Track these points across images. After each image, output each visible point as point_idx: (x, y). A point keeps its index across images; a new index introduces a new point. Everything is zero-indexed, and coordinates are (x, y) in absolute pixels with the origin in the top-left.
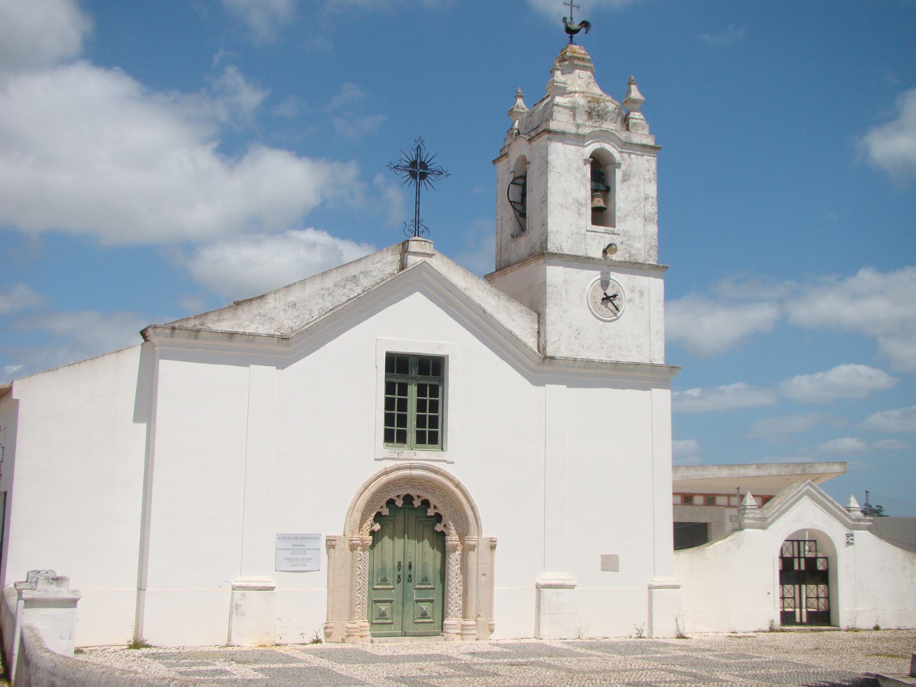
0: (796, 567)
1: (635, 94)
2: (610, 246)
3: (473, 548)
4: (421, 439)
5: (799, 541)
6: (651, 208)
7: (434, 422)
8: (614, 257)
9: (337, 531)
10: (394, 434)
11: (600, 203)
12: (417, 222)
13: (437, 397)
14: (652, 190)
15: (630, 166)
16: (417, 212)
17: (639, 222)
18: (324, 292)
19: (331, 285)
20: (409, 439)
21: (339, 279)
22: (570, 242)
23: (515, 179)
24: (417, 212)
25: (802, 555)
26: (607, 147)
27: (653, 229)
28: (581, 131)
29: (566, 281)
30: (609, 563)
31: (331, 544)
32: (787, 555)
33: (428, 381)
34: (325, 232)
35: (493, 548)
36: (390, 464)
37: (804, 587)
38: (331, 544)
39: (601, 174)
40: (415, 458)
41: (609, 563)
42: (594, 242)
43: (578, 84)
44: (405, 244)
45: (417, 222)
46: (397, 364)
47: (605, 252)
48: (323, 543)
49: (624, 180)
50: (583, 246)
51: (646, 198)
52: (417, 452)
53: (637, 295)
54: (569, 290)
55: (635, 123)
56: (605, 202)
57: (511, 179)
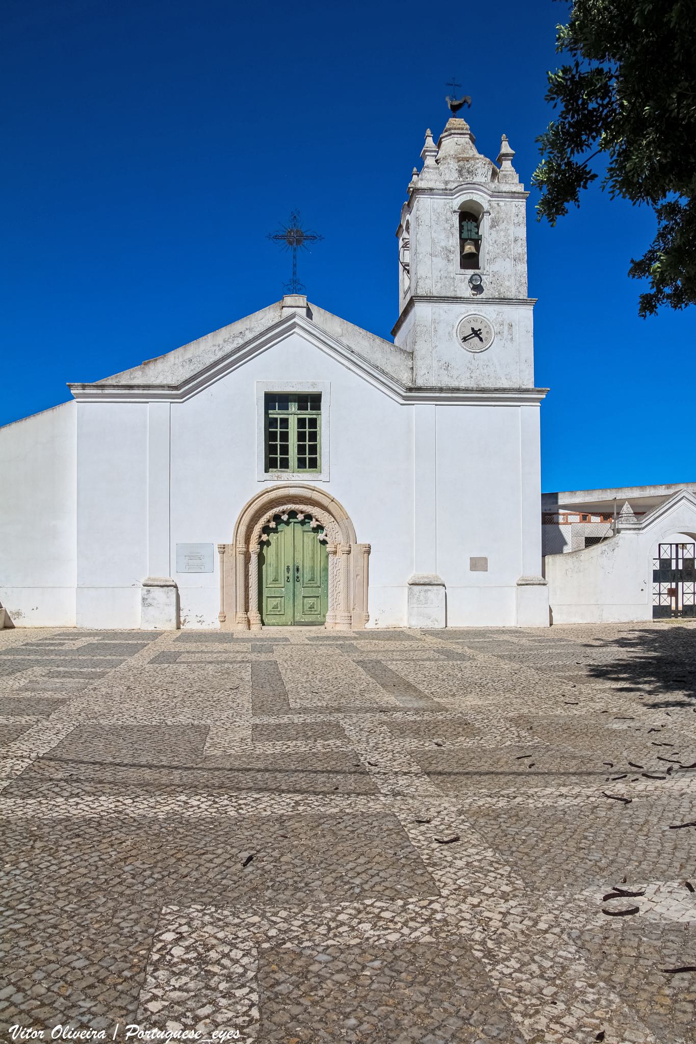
0: (674, 567)
1: (506, 148)
3: (584, 518)
4: (301, 464)
5: (677, 545)
6: (521, 249)
7: (313, 450)
9: (229, 541)
10: (274, 459)
11: (469, 248)
13: (276, 419)
14: (522, 232)
15: (498, 212)
17: (508, 264)
18: (214, 348)
19: (221, 342)
20: (291, 464)
21: (227, 336)
22: (439, 285)
25: (680, 556)
26: (476, 198)
27: (523, 268)
28: (449, 187)
29: (434, 321)
30: (479, 564)
31: (223, 549)
32: (665, 556)
33: (307, 415)
34: (578, 493)
35: (369, 552)
36: (270, 485)
37: (680, 584)
38: (223, 549)
40: (293, 480)
41: (479, 564)
46: (273, 400)
48: (216, 550)
49: (492, 227)
50: (452, 288)
51: (516, 240)
53: (506, 328)
54: (435, 329)
55: (505, 175)
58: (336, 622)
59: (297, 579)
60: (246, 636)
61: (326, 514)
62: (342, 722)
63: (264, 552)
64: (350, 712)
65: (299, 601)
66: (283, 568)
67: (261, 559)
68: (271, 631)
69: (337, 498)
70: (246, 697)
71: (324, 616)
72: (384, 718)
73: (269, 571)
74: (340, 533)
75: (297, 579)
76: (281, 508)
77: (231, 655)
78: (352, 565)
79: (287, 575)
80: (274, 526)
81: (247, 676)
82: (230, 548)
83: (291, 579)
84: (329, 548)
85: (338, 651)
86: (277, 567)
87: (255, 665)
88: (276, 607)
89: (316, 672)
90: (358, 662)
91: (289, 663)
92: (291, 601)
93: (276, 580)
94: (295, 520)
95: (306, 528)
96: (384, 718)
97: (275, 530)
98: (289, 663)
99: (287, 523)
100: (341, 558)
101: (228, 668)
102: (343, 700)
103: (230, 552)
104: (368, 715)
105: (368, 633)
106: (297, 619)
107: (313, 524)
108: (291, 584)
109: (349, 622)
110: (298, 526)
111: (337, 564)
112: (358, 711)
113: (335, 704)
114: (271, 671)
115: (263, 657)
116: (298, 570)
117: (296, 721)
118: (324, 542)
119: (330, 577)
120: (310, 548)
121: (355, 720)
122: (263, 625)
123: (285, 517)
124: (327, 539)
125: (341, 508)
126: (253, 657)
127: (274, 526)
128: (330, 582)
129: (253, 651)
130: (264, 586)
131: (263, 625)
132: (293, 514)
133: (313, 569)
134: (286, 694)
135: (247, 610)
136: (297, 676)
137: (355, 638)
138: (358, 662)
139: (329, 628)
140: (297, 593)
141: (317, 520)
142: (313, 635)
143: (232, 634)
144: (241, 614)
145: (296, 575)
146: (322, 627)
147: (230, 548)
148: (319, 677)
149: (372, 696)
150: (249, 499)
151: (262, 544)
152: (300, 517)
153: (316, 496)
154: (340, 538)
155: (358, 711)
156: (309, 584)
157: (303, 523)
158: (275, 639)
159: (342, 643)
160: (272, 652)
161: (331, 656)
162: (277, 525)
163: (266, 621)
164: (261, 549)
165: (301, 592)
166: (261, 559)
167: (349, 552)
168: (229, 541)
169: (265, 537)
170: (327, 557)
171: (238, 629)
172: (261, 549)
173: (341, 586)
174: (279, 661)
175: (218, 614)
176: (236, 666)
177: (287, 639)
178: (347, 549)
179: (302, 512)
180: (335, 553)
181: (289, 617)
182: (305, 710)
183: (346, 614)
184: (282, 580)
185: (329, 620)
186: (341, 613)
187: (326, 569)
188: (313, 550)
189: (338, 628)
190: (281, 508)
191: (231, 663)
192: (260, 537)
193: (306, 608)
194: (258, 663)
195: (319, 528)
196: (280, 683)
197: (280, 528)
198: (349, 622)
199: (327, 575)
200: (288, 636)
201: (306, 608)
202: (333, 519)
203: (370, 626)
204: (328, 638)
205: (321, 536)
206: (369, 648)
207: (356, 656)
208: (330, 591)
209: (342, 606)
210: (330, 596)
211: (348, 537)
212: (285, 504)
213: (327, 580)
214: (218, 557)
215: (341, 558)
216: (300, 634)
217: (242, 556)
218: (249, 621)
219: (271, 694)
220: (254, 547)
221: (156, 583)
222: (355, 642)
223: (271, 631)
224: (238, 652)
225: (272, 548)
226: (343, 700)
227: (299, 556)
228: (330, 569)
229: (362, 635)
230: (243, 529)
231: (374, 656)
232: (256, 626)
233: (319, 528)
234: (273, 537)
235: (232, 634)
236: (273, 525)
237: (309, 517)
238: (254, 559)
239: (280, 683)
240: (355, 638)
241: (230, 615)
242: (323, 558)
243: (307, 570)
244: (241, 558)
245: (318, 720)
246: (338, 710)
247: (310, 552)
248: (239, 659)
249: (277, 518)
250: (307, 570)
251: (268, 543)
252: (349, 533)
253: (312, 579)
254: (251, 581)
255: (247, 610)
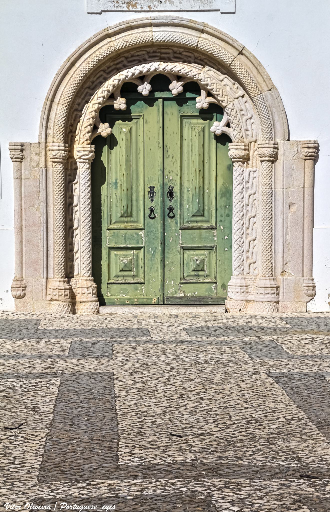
9: (33, 136)
31: (20, 152)
35: (315, 158)
38: (20, 152)
48: (6, 155)
58: (247, 299)
59: (169, 213)
60: (63, 325)
61: (228, 81)
62: (216, 495)
63: (104, 158)
64: (238, 476)
65: (173, 256)
66: (141, 191)
67: (98, 173)
68: (117, 316)
69: (251, 47)
70: (33, 445)
71: (224, 287)
72: (309, 490)
73: (113, 196)
74: (256, 119)
75: (169, 213)
76: (137, 70)
77: (25, 363)
78: (279, 186)
79: (149, 204)
80: (123, 106)
81: (46, 402)
82: (35, 150)
83: (158, 213)
84: (234, 150)
85: (242, 355)
86: (129, 190)
87: (67, 381)
88: (127, 268)
89: (187, 395)
90: (278, 378)
91: (137, 376)
92: (158, 257)
93: (127, 215)
94: (166, 94)
95: (187, 109)
96: (309, 490)
97: (125, 115)
98: (137, 376)
99: (150, 100)
100: (258, 169)
101: (13, 388)
102: (230, 452)
103: (34, 158)
104: (275, 483)
105: (311, 320)
106: (170, 292)
107: (202, 101)
108: (157, 223)
109: (273, 298)
110: (173, 109)
111: (250, 182)
112: (255, 473)
113: (210, 460)
114: (98, 393)
115: (89, 366)
116: (171, 194)
117: (123, 493)
118: (223, 139)
119: (235, 209)
120: (196, 151)
121: (244, 493)
122: (102, 302)
123: (145, 89)
124: (230, 132)
125: (257, 66)
126: (68, 366)
127: (123, 106)
128: (235, 219)
129: (72, 354)
130: (104, 226)
131: (102, 302)
132: (160, 81)
133: (201, 192)
134: (116, 438)
135: (69, 274)
136: (148, 402)
137: (283, 331)
138: (278, 378)
139: (233, 312)
140: (170, 240)
141: (209, 94)
142: (198, 323)
143: (38, 322)
144: (57, 282)
145: (168, 204)
146: (220, 310)
147: (35, 150)
148: (191, 404)
149: (292, 444)
150: (71, 50)
151: (99, 143)
152: (176, 87)
153: (206, 43)
154: (257, 130)
155: (255, 473)
156: (190, 222)
157: (180, 100)
158: (121, 332)
159: (254, 339)
160: (110, 356)
161: (226, 364)
162: (128, 104)
163: (107, 296)
164: (98, 153)
165: (177, 237)
166: (98, 173)
167: (274, 159)
168: (33, 136)
169: (104, 130)
170: (230, 168)
171: (52, 311)
172: (98, 153)
173: (258, 228)
174: (119, 373)
175: (10, 283)
176: (29, 383)
177: (144, 332)
178: (271, 151)
179: (179, 78)
180: (245, 160)
181: (153, 289)
182: (147, 471)
183: (268, 283)
184: (140, 215)
185: (233, 296)
186: (258, 279)
187: (227, 193)
188: (201, 155)
189: (251, 310)
190: (137, 70)
191: (21, 377)
192: (95, 128)
193: (188, 271)
194: (74, 377)
195: (214, 110)
196: (109, 415)
197: (135, 110)
198: (273, 298)
199: (229, 206)
200: (149, 325)
201: (188, 271)
202: (241, 92)
203: (319, 306)
204: (227, 329)
205: (218, 127)
206: (308, 349)
207: (277, 365)
208: (235, 237)
209: (260, 268)
210: (235, 246)
211: (272, 128)
212: (145, 61)
213: (229, 215)
214: (9, 168)
215: (258, 169)
216: (173, 322)
217: (59, 167)
218: (73, 296)
219: (86, 437)
220: (82, 148)
221: (45, 243)
222: (280, 339)
223: (117, 316)
224: (40, 356)
225: (120, 151)
226: (230, 452)
227: (173, 167)
228: (235, 192)
229: (297, 325)
230: (59, 112)
231: (313, 367)
232: (86, 307)
233: (214, 110)
234: (121, 129)
235: (38, 322)
236: (120, 103)
237: (193, 87)
238: (83, 172)
239: (109, 415)
240: (283, 331)
241: (35, 284)
242: (222, 169)
243: (189, 195)
244: (56, 171)
245: (170, 490)
246: (215, 471)
247: (196, 159)
248: (39, 370)
249: (128, 89)
250: (189, 195)
251: (111, 141)
252: (273, 116)
253: (200, 213)
254: (76, 216)
255: (69, 274)
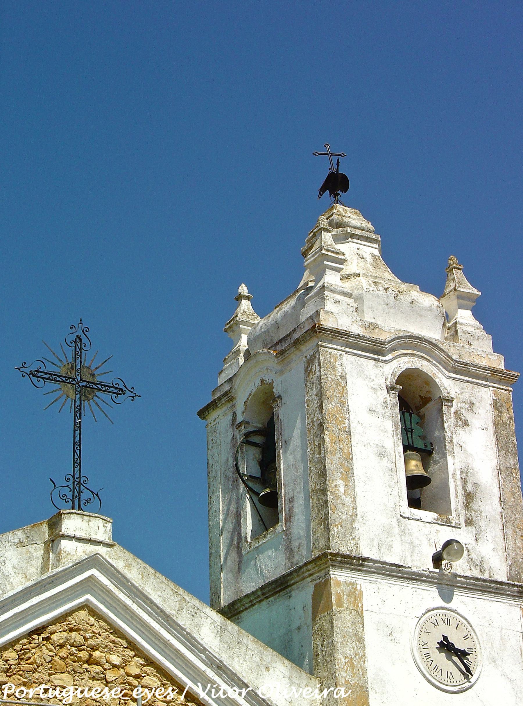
2: (448, 544)
8: (460, 567)
12: (77, 483)
16: (77, 462)
23: (247, 435)
24: (77, 462)
26: (427, 367)
39: (418, 409)
42: (419, 538)
43: (356, 281)
44: (54, 523)
45: (77, 483)
47: (437, 560)
52: (158, 630)
56: (425, 467)
57: (240, 439)
